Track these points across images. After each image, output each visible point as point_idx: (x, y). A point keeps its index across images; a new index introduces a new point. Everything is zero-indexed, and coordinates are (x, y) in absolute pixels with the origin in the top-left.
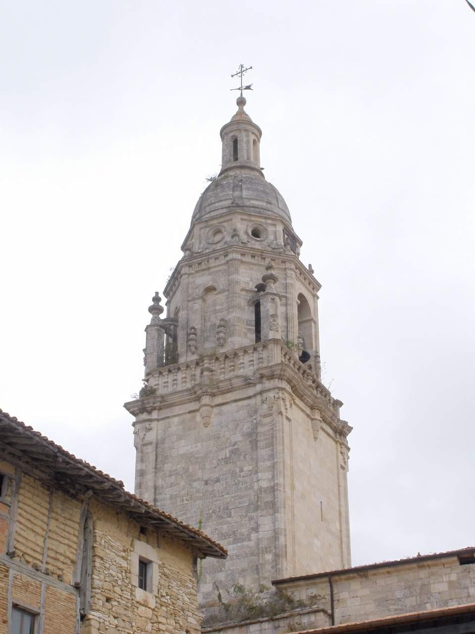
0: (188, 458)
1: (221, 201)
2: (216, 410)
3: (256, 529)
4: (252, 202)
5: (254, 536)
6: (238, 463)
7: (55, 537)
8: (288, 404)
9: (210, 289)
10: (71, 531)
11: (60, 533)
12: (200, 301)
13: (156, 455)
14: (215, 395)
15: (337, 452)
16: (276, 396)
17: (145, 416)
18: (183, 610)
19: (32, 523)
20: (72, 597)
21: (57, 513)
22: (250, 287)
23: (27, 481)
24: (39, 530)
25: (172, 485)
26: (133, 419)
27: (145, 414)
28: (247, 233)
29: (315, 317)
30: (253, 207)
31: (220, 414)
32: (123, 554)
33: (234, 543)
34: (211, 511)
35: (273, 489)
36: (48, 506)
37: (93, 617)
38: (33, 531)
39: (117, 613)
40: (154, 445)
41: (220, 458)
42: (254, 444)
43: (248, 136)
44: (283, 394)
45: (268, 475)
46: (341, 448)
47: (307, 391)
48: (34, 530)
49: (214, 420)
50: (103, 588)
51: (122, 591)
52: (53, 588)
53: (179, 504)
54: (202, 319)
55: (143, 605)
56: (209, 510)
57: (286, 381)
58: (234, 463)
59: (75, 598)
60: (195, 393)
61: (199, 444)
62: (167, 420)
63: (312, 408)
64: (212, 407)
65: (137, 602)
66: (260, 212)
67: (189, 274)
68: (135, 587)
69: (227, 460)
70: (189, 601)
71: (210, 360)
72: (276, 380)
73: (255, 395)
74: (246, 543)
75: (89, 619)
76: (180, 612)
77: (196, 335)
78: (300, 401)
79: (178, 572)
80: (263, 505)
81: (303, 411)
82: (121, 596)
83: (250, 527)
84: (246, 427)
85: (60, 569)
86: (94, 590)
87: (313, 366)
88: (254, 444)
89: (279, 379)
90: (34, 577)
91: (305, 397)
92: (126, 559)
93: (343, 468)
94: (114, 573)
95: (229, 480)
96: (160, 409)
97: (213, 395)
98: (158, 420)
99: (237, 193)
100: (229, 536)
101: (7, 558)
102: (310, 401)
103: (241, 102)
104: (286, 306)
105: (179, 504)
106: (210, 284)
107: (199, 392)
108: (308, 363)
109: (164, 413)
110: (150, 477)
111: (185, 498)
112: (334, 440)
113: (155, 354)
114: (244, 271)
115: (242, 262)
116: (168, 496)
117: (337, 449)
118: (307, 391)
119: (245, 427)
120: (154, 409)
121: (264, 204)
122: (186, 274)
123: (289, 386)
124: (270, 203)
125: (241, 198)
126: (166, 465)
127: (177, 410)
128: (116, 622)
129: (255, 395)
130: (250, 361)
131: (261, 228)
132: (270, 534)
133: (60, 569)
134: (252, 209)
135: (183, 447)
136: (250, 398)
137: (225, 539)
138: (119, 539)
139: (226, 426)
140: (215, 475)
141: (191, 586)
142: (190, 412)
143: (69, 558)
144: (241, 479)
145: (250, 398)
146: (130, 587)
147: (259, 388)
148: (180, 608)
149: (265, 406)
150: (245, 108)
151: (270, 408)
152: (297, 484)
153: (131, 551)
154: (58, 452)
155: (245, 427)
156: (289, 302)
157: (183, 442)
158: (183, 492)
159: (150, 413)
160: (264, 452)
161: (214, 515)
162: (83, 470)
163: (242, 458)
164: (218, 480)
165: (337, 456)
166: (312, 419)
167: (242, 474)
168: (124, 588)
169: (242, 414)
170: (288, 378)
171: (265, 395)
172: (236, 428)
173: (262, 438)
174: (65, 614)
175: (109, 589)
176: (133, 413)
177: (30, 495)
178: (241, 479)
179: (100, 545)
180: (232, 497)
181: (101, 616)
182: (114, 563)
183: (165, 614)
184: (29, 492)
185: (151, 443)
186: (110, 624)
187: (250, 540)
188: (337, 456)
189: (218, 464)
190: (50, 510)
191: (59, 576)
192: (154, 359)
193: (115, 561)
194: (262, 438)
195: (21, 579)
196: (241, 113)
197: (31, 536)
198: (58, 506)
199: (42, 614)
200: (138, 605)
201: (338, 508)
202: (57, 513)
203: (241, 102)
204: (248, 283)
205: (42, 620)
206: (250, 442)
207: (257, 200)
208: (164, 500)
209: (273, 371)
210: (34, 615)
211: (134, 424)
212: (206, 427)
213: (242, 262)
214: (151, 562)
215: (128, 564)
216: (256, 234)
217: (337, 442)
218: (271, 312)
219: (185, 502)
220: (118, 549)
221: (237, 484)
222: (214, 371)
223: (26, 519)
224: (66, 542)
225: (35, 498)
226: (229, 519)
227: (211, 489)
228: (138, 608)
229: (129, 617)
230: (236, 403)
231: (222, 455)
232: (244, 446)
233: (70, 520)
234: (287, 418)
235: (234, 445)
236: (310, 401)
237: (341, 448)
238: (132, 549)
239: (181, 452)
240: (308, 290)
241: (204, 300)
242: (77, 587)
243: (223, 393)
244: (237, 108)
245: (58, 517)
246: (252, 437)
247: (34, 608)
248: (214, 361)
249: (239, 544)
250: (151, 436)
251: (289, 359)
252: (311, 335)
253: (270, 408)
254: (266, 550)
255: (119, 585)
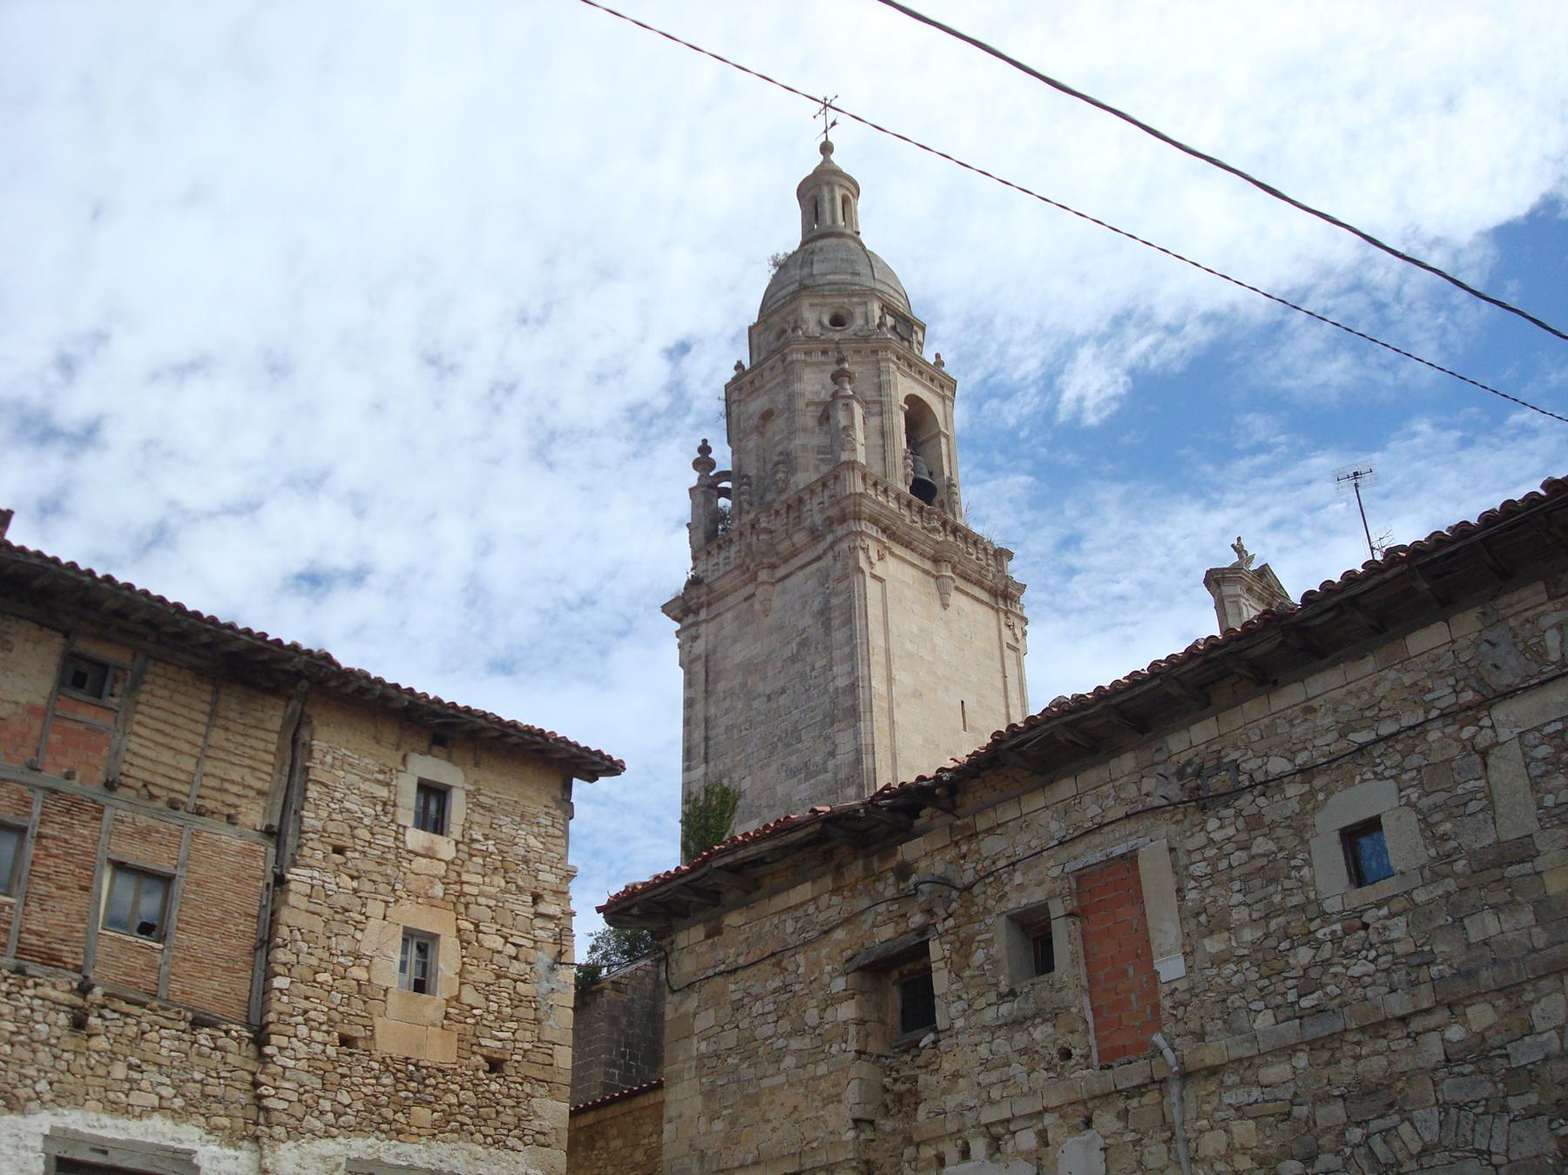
0: (752, 667)
1: (783, 288)
2: (778, 587)
3: (832, 754)
4: (828, 277)
5: (831, 764)
6: (808, 660)
7: (222, 755)
8: (874, 556)
9: (767, 416)
10: (261, 745)
11: (232, 750)
12: (755, 436)
13: (706, 672)
14: (776, 567)
15: (999, 624)
16: (852, 545)
17: (690, 619)
18: (526, 861)
19: (167, 735)
20: (256, 847)
21: (227, 718)
22: (822, 396)
23: (160, 671)
24: (186, 747)
25: (727, 711)
26: (677, 626)
27: (691, 616)
28: (820, 323)
29: (947, 428)
30: (829, 284)
31: (783, 592)
32: (381, 777)
33: (806, 780)
34: (776, 739)
35: (853, 688)
36: (207, 708)
37: (296, 877)
38: (171, 748)
39: (357, 871)
40: (703, 659)
41: (785, 656)
42: (827, 627)
43: (832, 191)
44: (862, 540)
45: (846, 668)
46: (1008, 618)
47: (915, 534)
48: (172, 746)
49: (776, 603)
50: (325, 831)
51: (372, 834)
52: (209, 835)
53: (736, 737)
54: (758, 460)
55: (424, 856)
56: (773, 737)
57: (869, 521)
58: (803, 660)
59: (263, 849)
60: (748, 569)
61: (759, 643)
62: (717, 620)
63: (936, 560)
64: (773, 584)
65: (409, 852)
66: (841, 289)
67: (739, 401)
68: (405, 827)
69: (794, 659)
70: (542, 846)
71: (767, 517)
72: (852, 522)
73: (825, 553)
74: (821, 777)
75: (289, 881)
76: (518, 865)
77: (750, 486)
78: (908, 552)
79: (516, 802)
80: (841, 715)
81: (914, 565)
82: (370, 842)
83: (826, 751)
84: (816, 604)
85: (230, 805)
86: (304, 836)
87: (945, 501)
88: (827, 627)
89: (854, 519)
90: (164, 819)
91: (916, 543)
92: (388, 785)
93: (1015, 649)
94: (354, 808)
95: (797, 686)
96: (709, 604)
97: (773, 567)
98: (707, 621)
99: (806, 271)
100: (800, 771)
101: (102, 790)
102: (928, 549)
103: (826, 148)
104: (881, 414)
105: (736, 737)
106: (767, 407)
107: (752, 566)
108: (936, 500)
109: (715, 609)
110: (699, 706)
111: (743, 727)
112: (993, 608)
113: (702, 527)
114: (812, 376)
115: (806, 363)
116: (723, 728)
117: (999, 621)
118: (915, 534)
119: (816, 603)
120: (701, 606)
121: (849, 277)
122: (735, 401)
123: (875, 528)
124: (858, 274)
125: (812, 275)
126: (719, 684)
127: (730, 600)
128: (355, 884)
129: (825, 553)
130: (819, 504)
131: (843, 312)
132: (851, 757)
133: (230, 805)
134: (827, 287)
135: (739, 653)
136: (819, 558)
137: (795, 776)
138: (370, 754)
139: (792, 608)
140: (781, 683)
141: (549, 823)
142: (746, 599)
143: (250, 787)
144: (812, 682)
145: (819, 558)
146: (394, 827)
147: (830, 538)
148: (520, 858)
149: (839, 565)
150: (833, 157)
151: (845, 566)
152: (898, 674)
153: (398, 771)
154: (176, 612)
155: (816, 603)
156: (886, 408)
157: (739, 646)
158: (740, 720)
159: (696, 613)
160: (839, 636)
161: (779, 744)
162: (238, 639)
163: (813, 650)
164: (783, 691)
165: (1000, 631)
166: (937, 578)
167: (814, 674)
168: (376, 829)
169: (812, 583)
170: (870, 516)
171: (837, 548)
172: (804, 608)
173: (837, 613)
174: (238, 875)
175: (341, 832)
176: (675, 619)
177: (166, 693)
178: (812, 682)
179: (322, 763)
180: (801, 712)
181: (316, 874)
182: (355, 791)
183: (480, 870)
184: (165, 687)
185: (699, 657)
186: (339, 888)
187: (826, 772)
188: (1000, 631)
189: (783, 667)
190: (213, 715)
191: (229, 817)
192: (701, 534)
193: (359, 789)
194: (837, 613)
195: (134, 823)
196: (827, 161)
197: (166, 757)
198: (231, 707)
199: (180, 876)
200: (411, 856)
201: (1003, 711)
202: (227, 718)
203: (826, 148)
204: (818, 393)
205: (177, 889)
206: (822, 624)
207: (835, 273)
208: (717, 735)
209: (843, 510)
210: (166, 880)
211: (678, 634)
212: (767, 616)
213: (806, 363)
214: (450, 787)
215: (390, 792)
216: (837, 321)
217: (997, 611)
218: (843, 422)
219: (744, 733)
220: (366, 770)
221: (807, 690)
222: (775, 531)
223: (152, 729)
224: (247, 762)
225: (177, 697)
226: (799, 746)
227: (775, 706)
228: (411, 861)
229: (387, 875)
230: (803, 572)
231: (787, 653)
232: (816, 632)
233: (257, 727)
234: (874, 577)
235: (802, 634)
236: (928, 549)
237: (1008, 618)
238: (402, 768)
239: (736, 662)
240: (925, 386)
241: (762, 434)
242: (269, 832)
243: (786, 561)
244: (821, 157)
245: (231, 725)
246: (824, 614)
247: (165, 867)
248: (772, 517)
249: (813, 781)
250: (700, 647)
251: (885, 491)
252: (941, 454)
253: (845, 566)
254: (847, 782)
255: (366, 826)
